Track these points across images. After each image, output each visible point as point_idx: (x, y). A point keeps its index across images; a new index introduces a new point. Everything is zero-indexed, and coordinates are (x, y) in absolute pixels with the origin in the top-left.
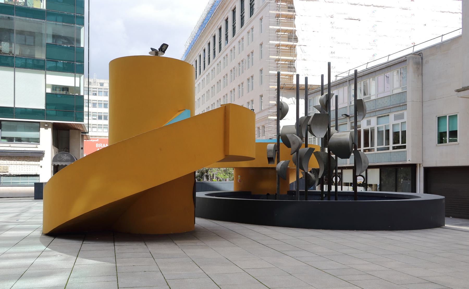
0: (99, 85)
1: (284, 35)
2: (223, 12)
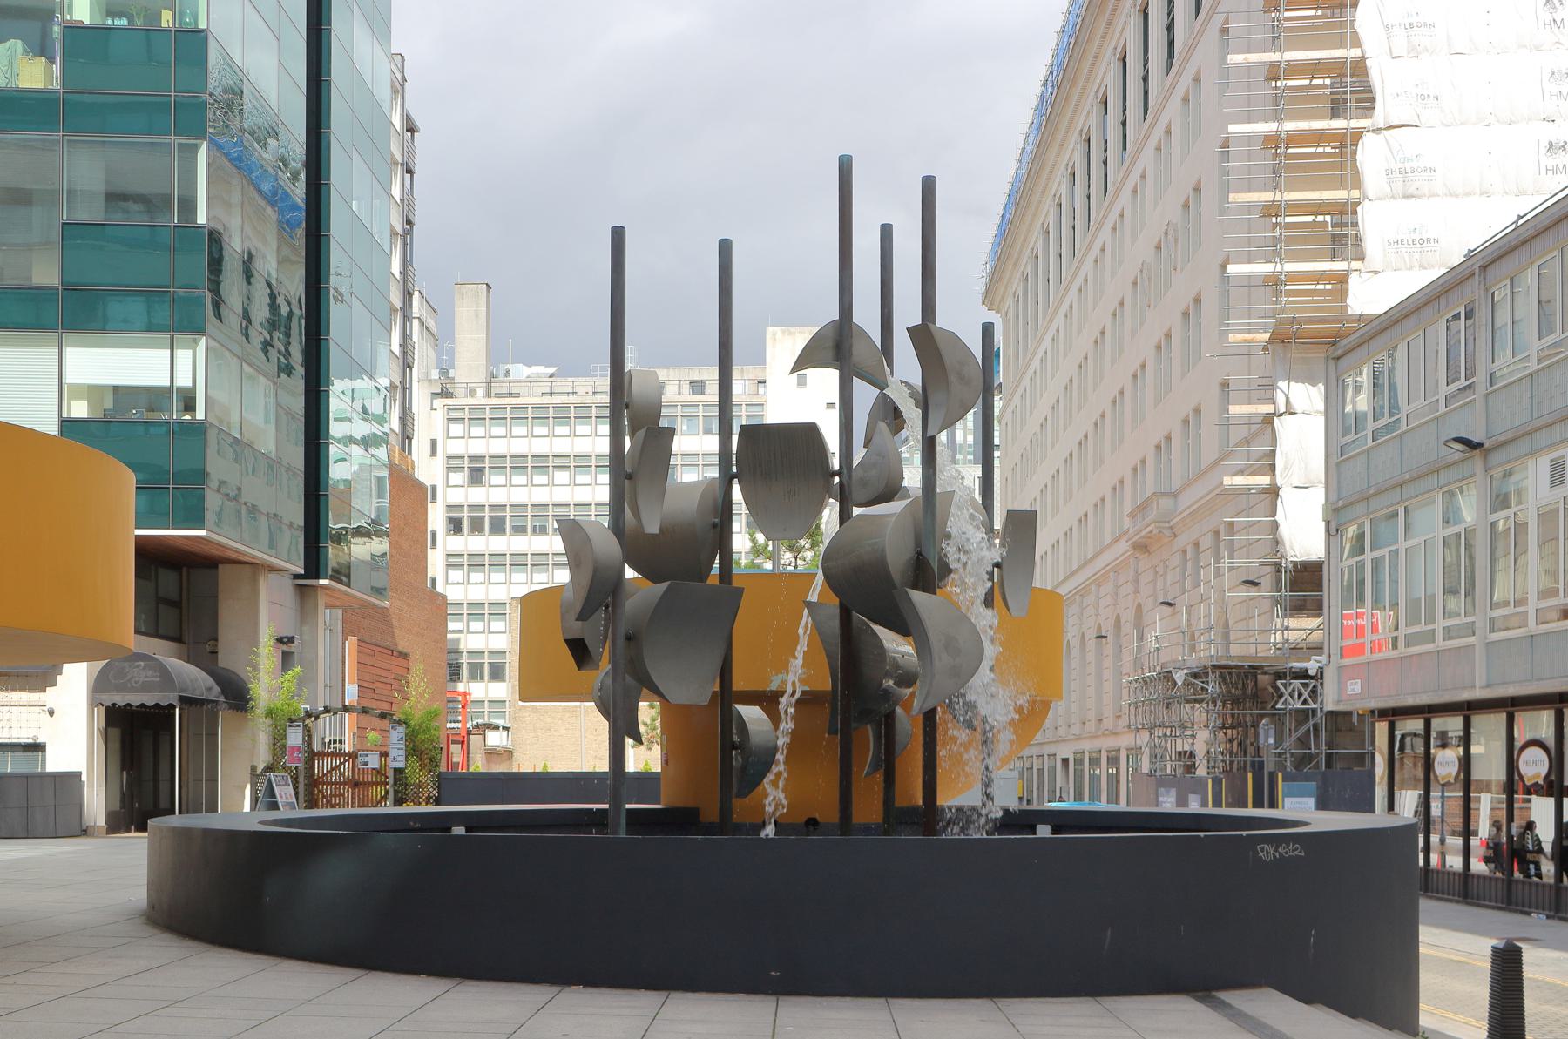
0: (686, 388)
1: (1310, 86)
2: (1109, 23)
